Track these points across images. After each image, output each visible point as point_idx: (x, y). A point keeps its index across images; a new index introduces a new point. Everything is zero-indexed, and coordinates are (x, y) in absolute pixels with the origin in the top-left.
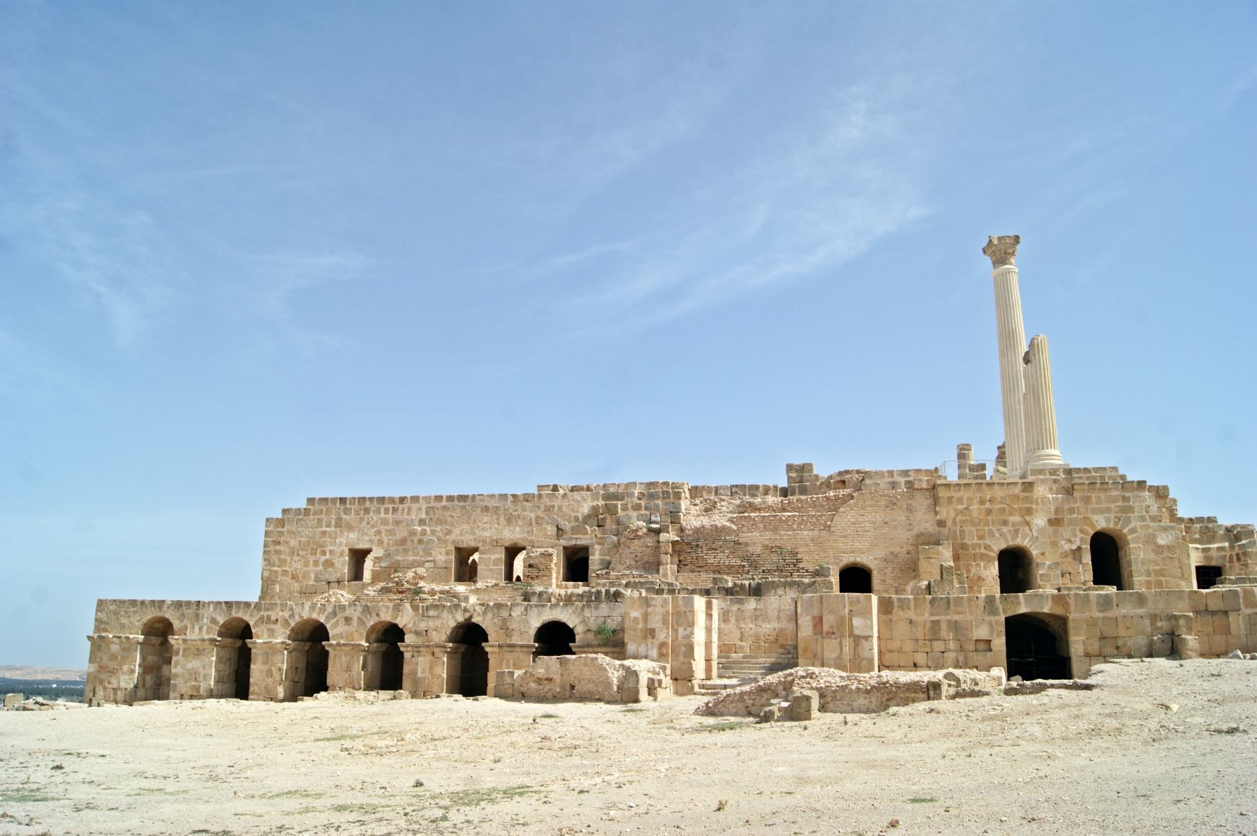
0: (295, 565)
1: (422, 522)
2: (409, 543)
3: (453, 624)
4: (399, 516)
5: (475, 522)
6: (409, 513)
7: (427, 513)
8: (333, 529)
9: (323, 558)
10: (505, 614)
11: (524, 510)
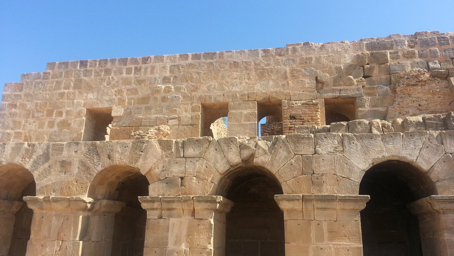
0: (29, 127)
1: (166, 80)
2: (152, 101)
3: (222, 167)
5: (223, 78)
6: (152, 72)
7: (171, 71)
8: (71, 90)
9: (59, 119)
10: (308, 150)
11: (278, 63)
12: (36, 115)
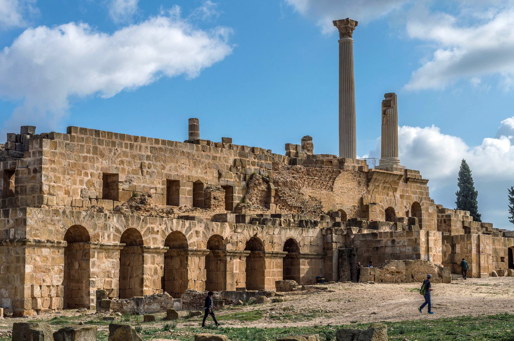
1: (148, 157)
4: (136, 152)
8: (91, 155)
9: (86, 179)
12: (70, 172)
